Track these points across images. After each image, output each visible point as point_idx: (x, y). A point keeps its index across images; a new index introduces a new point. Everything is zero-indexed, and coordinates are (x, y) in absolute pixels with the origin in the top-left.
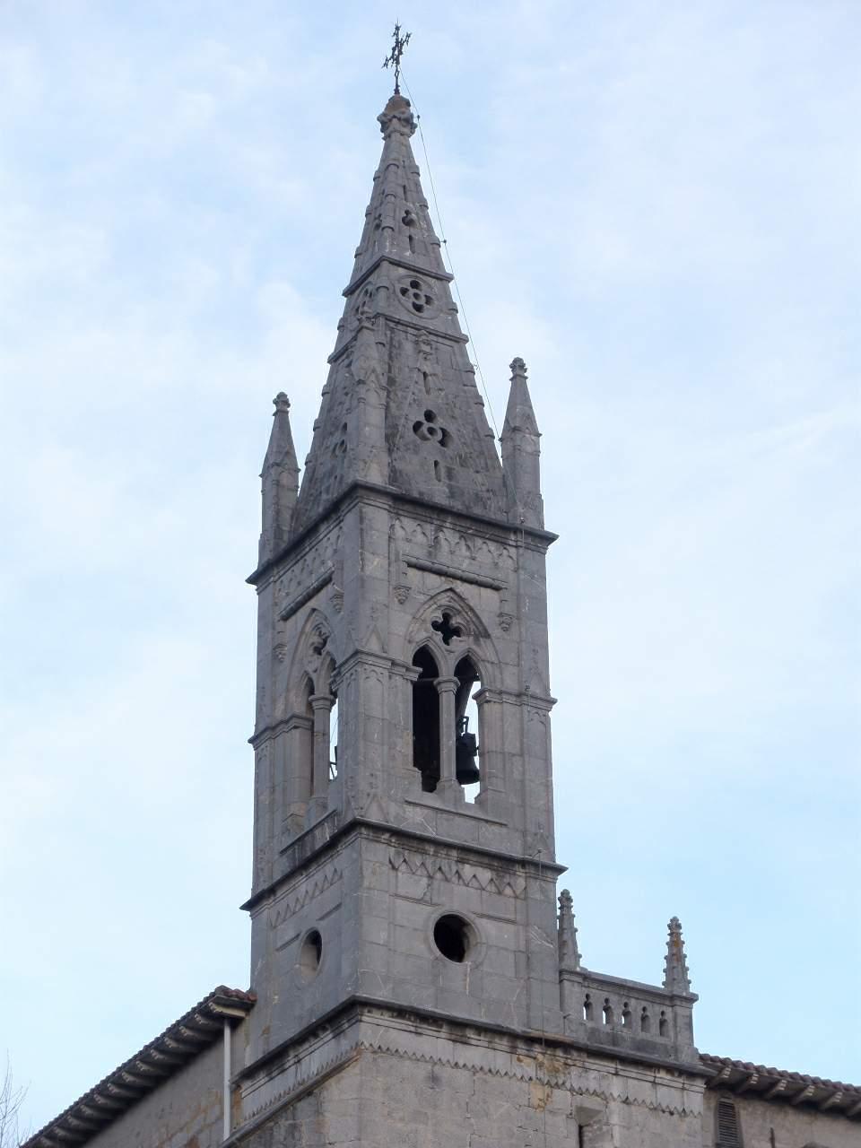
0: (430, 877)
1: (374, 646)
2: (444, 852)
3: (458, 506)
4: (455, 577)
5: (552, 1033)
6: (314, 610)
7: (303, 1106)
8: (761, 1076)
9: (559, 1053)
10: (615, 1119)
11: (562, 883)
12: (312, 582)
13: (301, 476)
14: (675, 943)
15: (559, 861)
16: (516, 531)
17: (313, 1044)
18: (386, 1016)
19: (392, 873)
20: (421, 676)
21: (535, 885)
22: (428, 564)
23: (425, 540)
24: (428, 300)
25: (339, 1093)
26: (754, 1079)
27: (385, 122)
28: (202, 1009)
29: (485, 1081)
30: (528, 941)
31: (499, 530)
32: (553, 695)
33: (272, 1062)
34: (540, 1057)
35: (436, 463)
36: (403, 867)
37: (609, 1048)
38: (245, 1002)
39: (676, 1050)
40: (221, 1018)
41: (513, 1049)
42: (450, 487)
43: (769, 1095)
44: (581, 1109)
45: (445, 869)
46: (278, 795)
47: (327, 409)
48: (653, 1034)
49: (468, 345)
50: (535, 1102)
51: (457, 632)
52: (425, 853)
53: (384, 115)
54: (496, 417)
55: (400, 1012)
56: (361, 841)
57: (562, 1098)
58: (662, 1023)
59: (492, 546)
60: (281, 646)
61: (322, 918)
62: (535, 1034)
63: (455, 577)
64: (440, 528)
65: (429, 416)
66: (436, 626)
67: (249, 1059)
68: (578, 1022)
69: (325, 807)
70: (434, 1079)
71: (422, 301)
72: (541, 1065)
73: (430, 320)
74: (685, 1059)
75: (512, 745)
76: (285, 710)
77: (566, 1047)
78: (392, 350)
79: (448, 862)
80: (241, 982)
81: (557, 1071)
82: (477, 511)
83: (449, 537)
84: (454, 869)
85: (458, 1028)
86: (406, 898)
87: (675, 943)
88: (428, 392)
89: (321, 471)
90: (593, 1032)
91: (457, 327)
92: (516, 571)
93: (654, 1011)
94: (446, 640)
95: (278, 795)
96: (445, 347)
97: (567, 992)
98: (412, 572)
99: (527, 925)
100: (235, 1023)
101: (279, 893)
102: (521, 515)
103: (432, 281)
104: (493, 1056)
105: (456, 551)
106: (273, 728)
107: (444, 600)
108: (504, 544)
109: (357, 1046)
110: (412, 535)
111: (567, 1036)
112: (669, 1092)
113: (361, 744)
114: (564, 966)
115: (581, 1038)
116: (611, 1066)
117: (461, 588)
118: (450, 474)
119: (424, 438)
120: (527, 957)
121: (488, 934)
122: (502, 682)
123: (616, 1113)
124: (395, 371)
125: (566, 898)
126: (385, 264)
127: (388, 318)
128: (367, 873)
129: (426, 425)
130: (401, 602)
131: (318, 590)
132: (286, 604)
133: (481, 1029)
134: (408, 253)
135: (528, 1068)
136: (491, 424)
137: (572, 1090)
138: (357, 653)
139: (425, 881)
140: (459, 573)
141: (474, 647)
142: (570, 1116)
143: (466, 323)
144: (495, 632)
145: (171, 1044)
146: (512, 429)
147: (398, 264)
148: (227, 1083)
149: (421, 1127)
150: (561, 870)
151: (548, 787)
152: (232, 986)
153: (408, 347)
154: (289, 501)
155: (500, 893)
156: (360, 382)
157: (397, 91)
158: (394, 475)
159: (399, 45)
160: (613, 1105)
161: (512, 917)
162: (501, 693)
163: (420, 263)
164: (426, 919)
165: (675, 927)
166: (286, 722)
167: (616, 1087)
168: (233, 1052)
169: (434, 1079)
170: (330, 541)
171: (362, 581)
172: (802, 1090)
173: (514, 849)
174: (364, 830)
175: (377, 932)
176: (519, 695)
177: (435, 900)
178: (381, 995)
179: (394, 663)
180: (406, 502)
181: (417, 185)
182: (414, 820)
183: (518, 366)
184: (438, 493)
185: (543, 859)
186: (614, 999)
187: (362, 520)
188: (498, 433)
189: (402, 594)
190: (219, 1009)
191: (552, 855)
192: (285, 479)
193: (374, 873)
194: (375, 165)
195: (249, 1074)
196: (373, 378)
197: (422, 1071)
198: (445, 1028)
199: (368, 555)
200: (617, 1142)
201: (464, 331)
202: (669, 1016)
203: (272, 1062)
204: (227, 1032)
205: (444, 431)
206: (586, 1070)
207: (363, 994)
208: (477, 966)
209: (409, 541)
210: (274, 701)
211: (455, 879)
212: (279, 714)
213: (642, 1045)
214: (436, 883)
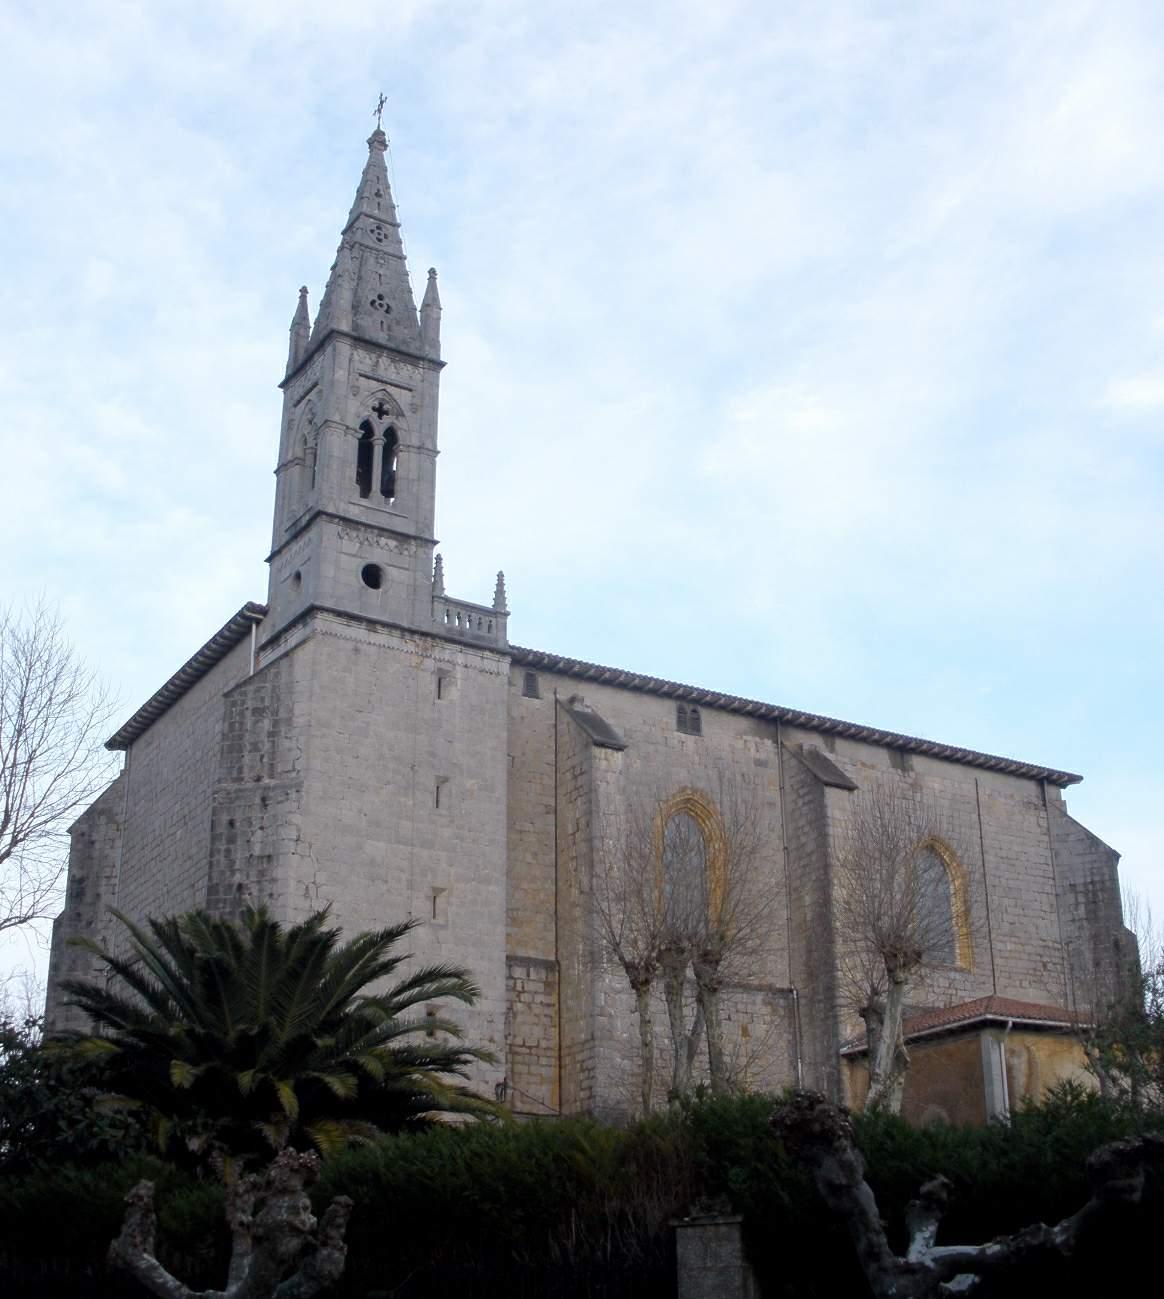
0: (361, 543)
1: (337, 418)
2: (369, 530)
3: (391, 345)
4: (386, 383)
5: (425, 628)
6: (309, 400)
7: (284, 663)
8: (581, 667)
9: (429, 639)
10: (459, 676)
11: (436, 550)
12: (309, 385)
13: (311, 330)
14: (500, 584)
15: (436, 538)
16: (423, 359)
17: (295, 630)
18: (331, 615)
19: (339, 540)
20: (364, 435)
21: (421, 551)
22: (370, 374)
23: (370, 362)
24: (386, 236)
25: (301, 655)
26: (546, 661)
27: (370, 142)
28: (240, 614)
29: (385, 652)
30: (415, 580)
31: (413, 359)
32: (439, 449)
33: (274, 641)
34: (418, 641)
35: (382, 322)
36: (346, 537)
37: (457, 637)
38: (264, 611)
39: (496, 641)
40: (250, 619)
41: (402, 637)
42: (389, 335)
43: (555, 669)
44: (440, 670)
45: (370, 539)
46: (286, 502)
47: (328, 295)
48: (484, 632)
49: (406, 261)
50: (414, 664)
51: (386, 413)
52: (358, 530)
53: (370, 139)
54: (418, 300)
55: (339, 614)
56: (322, 522)
57: (429, 663)
58: (490, 627)
59: (410, 367)
60: (293, 420)
61: (303, 565)
62: (414, 628)
63: (386, 383)
64: (380, 356)
65: (380, 297)
66: (374, 409)
67: (264, 640)
68: (443, 621)
69: (307, 506)
70: (356, 650)
71: (382, 237)
72: (418, 646)
73: (385, 246)
74: (501, 645)
75: (413, 475)
76: (293, 454)
77: (433, 636)
78: (362, 262)
79: (372, 536)
80: (262, 600)
81: (427, 649)
82: (403, 348)
83: (384, 361)
84: (375, 539)
85: (372, 624)
86: (345, 554)
87: (500, 584)
88: (381, 284)
89: (322, 326)
90: (450, 630)
91: (401, 251)
92: (423, 381)
93: (485, 620)
94: (380, 417)
95: (286, 502)
96: (393, 262)
97: (435, 608)
98: (362, 379)
99: (415, 571)
100: (258, 622)
101: (283, 553)
102: (428, 352)
103: (388, 226)
104: (394, 640)
105: (387, 368)
106: (286, 465)
107: (380, 395)
108: (416, 366)
109: (314, 631)
110: (364, 359)
111: (434, 631)
112: (490, 662)
113: (326, 470)
114: (435, 594)
115: (443, 632)
116: (458, 647)
117: (390, 389)
118: (389, 329)
119: (376, 308)
120: (414, 589)
121: (392, 575)
122: (410, 441)
123: (459, 673)
124: (363, 273)
125: (439, 558)
126: (362, 216)
127: (361, 245)
128: (325, 538)
129: (378, 302)
130: (355, 395)
131: (311, 389)
132: (297, 397)
133: (385, 625)
134: (376, 211)
135: (411, 647)
136: (415, 303)
137: (434, 659)
138: (326, 421)
139: (358, 545)
140: (389, 381)
141: (395, 421)
142: (433, 673)
143: (406, 249)
144: (408, 413)
145: (227, 633)
146: (426, 305)
147: (371, 217)
148: (252, 654)
149: (347, 674)
150: (436, 543)
151: (432, 498)
152: (257, 602)
153: (372, 261)
154: (303, 343)
155: (401, 554)
156: (340, 276)
157: (379, 127)
158: (356, 326)
159: (382, 103)
160: (458, 668)
161: (407, 566)
162: (409, 446)
163: (383, 217)
164: (358, 565)
165: (500, 576)
166: (292, 461)
167: (460, 659)
168: (258, 636)
169: (356, 650)
170: (319, 361)
171: (332, 383)
172: (573, 667)
173: (411, 531)
174: (324, 516)
175: (329, 571)
176: (419, 448)
177: (363, 556)
178: (328, 604)
179: (348, 428)
180: (360, 341)
181: (386, 176)
182: (354, 512)
183: (432, 272)
184: (382, 337)
185: (427, 536)
186: (463, 612)
187: (334, 350)
188: (419, 309)
189: (355, 391)
190: (249, 614)
191: (432, 534)
192: (302, 331)
193: (329, 539)
194: (364, 165)
195: (263, 648)
196: (347, 274)
197: (350, 646)
198: (364, 624)
199: (336, 369)
200: (459, 687)
201: (405, 254)
202: (494, 623)
203: (274, 641)
204: (254, 627)
205: (389, 307)
206: (444, 649)
207: (317, 603)
208: (386, 592)
209: (361, 362)
210: (287, 451)
211: (375, 545)
212: (290, 457)
213: (478, 638)
214: (364, 547)
